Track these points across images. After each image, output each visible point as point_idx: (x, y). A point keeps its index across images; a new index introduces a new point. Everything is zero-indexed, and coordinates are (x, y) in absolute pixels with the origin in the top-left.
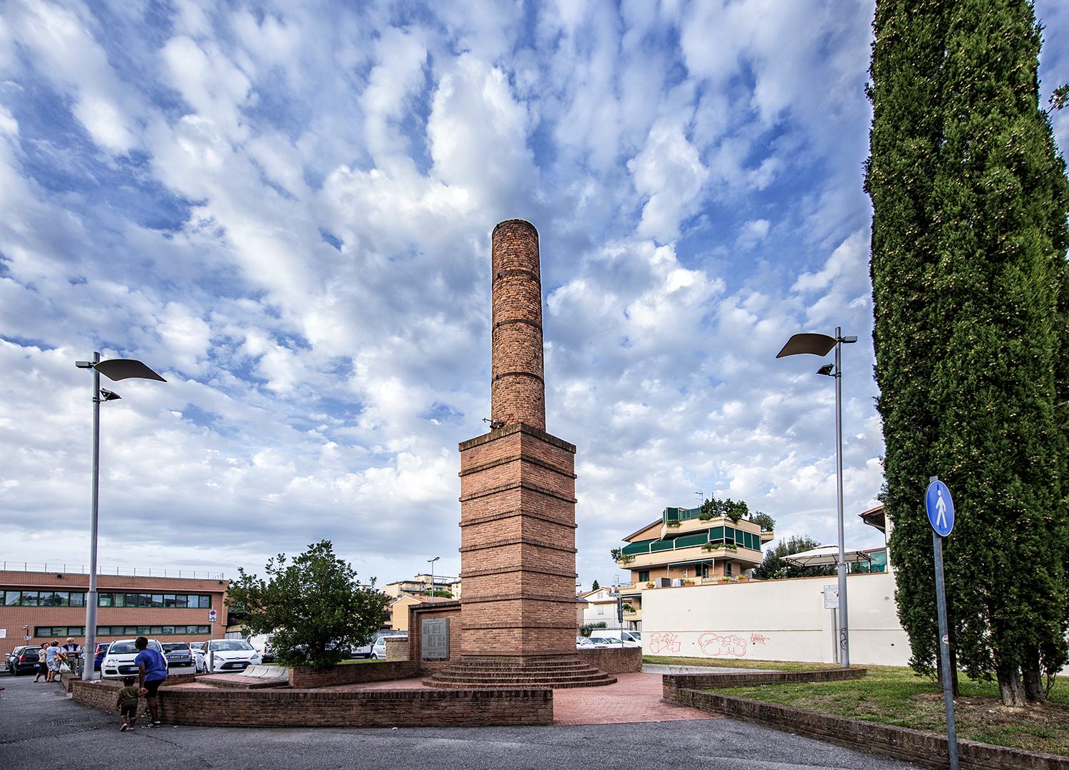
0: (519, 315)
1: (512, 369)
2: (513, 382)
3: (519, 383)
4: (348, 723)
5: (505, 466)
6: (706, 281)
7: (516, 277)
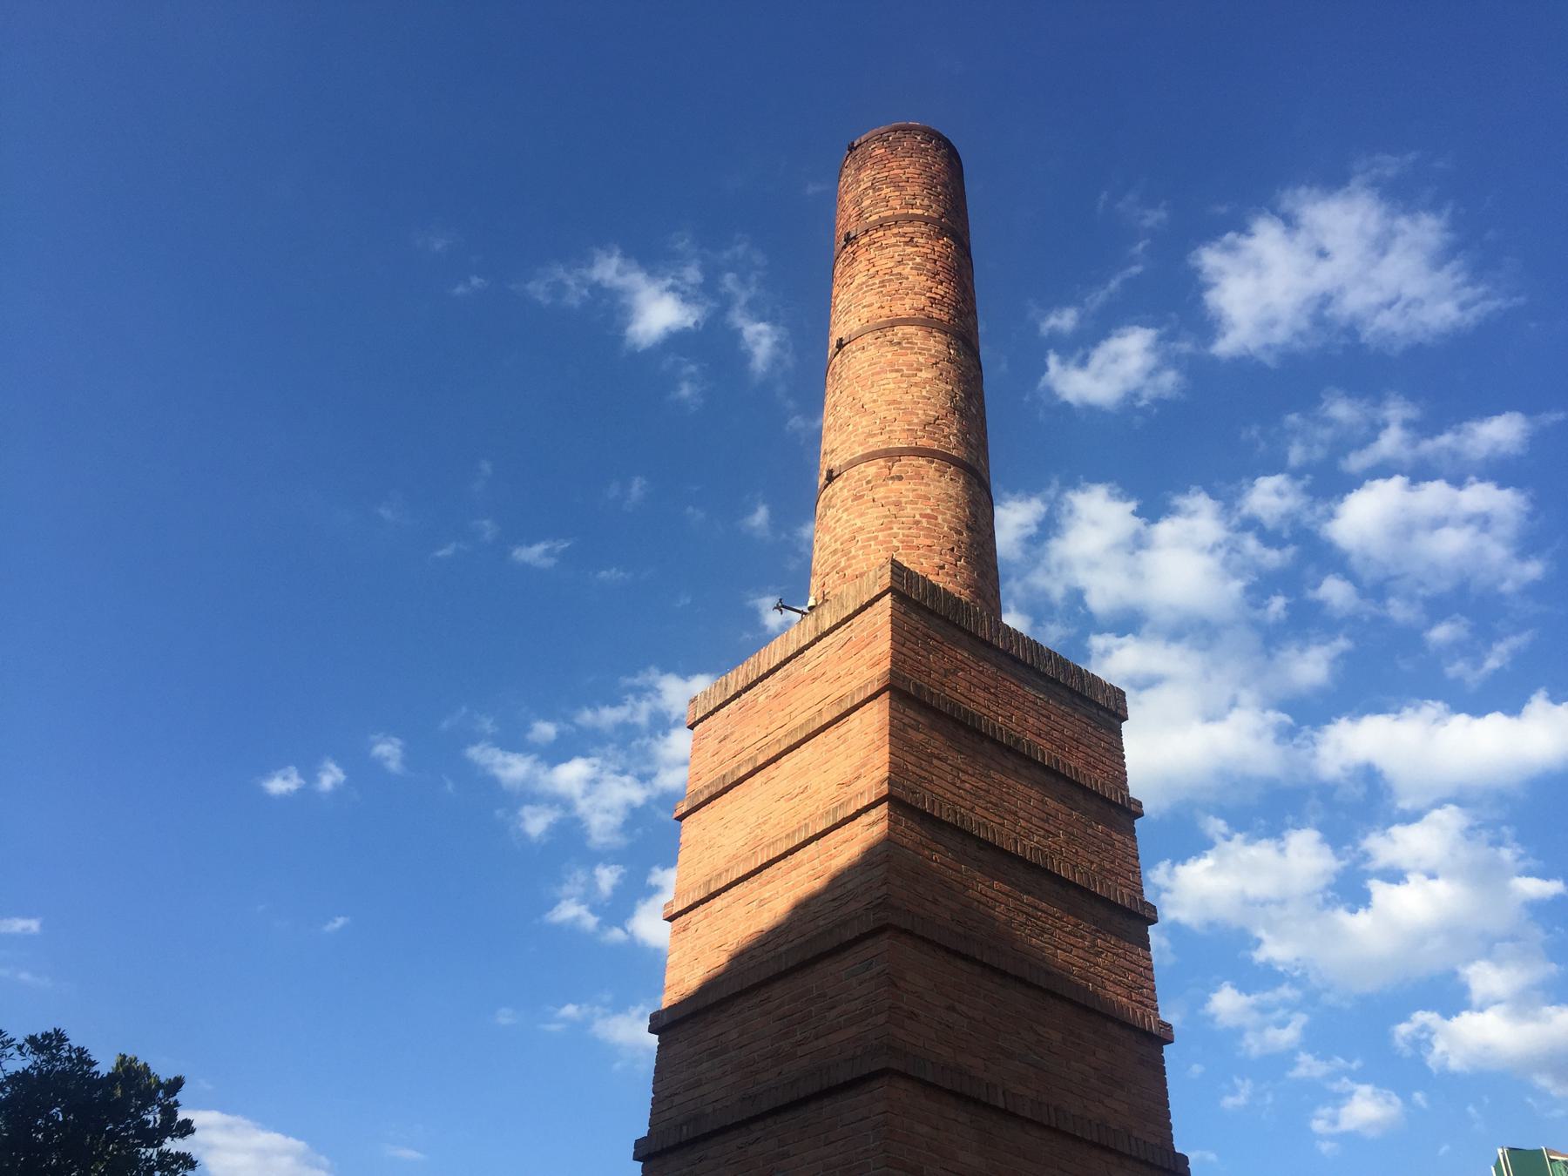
0: (904, 307)
1: (877, 443)
2: (877, 475)
3: (900, 478)
6: (1393, 716)
7: (895, 231)
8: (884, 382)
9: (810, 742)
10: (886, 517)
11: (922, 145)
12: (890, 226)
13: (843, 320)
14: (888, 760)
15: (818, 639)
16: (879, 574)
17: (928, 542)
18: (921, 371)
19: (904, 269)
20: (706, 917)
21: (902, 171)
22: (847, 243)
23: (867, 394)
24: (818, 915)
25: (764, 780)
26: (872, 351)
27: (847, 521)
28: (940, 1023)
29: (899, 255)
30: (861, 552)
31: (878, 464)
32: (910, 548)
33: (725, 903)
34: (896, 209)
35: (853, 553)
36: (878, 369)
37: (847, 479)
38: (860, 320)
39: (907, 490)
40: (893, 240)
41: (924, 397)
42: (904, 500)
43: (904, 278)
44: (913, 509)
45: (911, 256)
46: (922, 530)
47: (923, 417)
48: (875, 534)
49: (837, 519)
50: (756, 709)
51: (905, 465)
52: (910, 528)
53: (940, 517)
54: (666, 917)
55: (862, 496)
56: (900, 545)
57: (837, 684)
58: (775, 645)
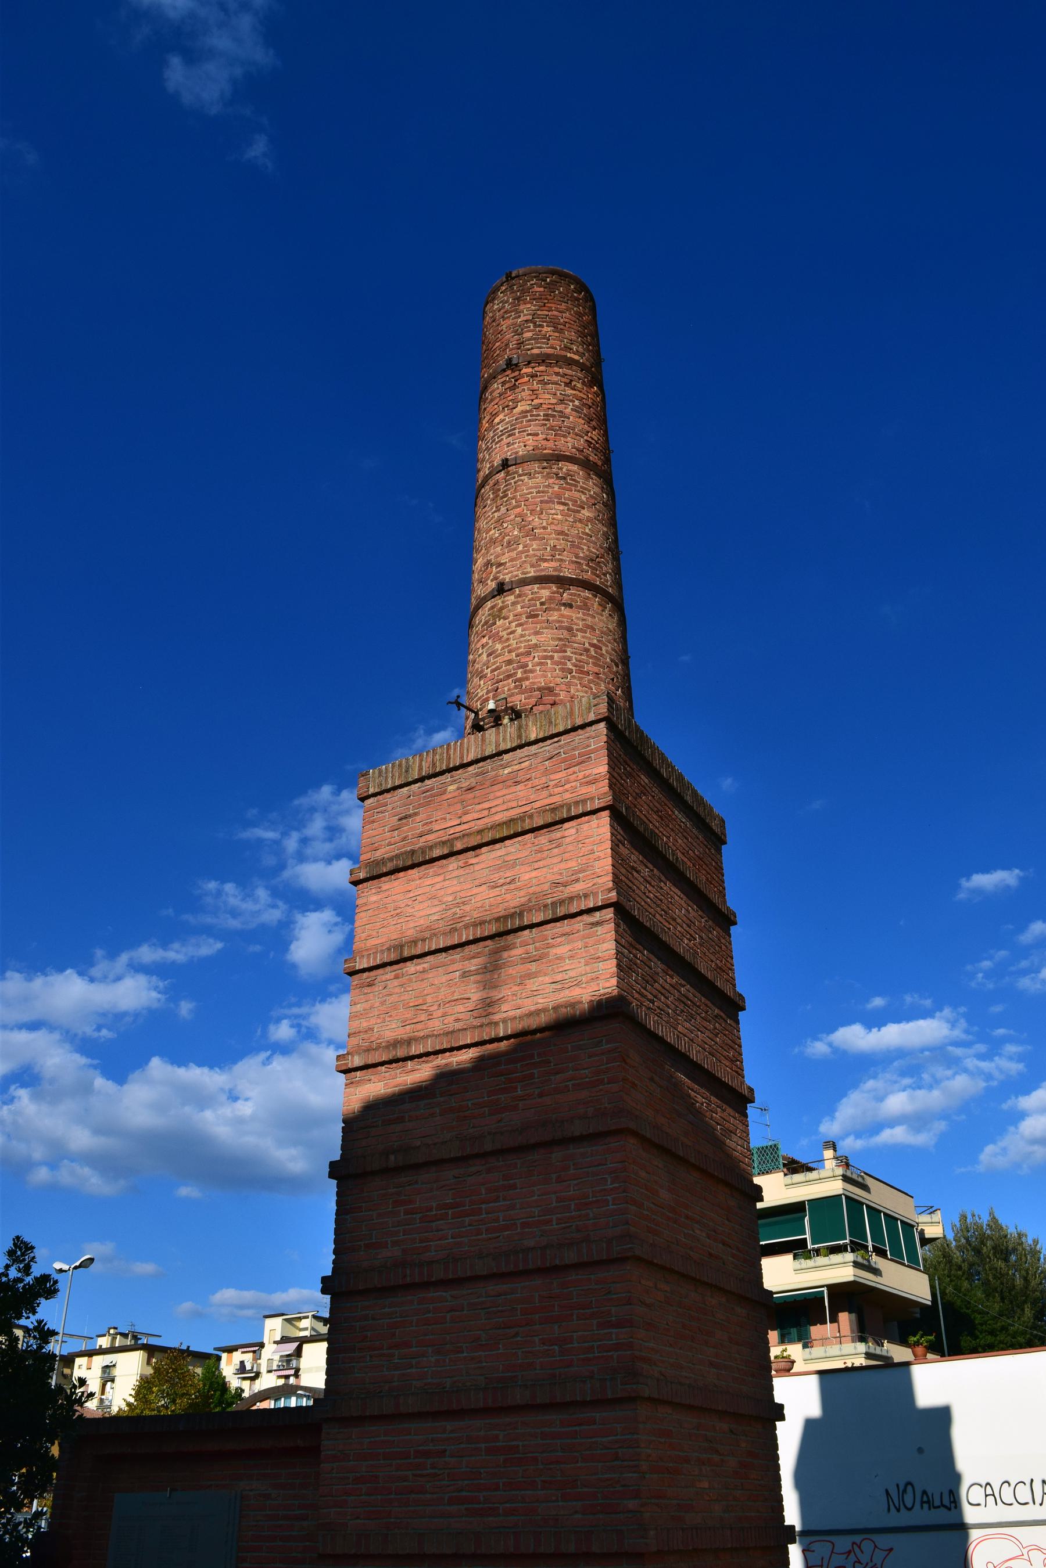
0: (569, 444)
1: (548, 568)
2: (551, 599)
3: (571, 606)
4: (450, 898)
5: (543, 839)
7: (557, 369)
8: (553, 511)
9: (516, 839)
10: (560, 639)
11: (575, 295)
12: (551, 363)
13: (505, 441)
14: (611, 871)
15: (521, 747)
16: (595, 702)
17: (596, 669)
18: (584, 508)
19: (565, 408)
20: (396, 977)
21: (560, 314)
22: (507, 368)
23: (537, 519)
24: (535, 993)
25: (461, 863)
26: (539, 478)
27: (522, 636)
28: (647, 1091)
29: (561, 394)
30: (538, 668)
31: (550, 588)
32: (582, 672)
33: (420, 968)
34: (556, 349)
35: (530, 667)
36: (546, 498)
37: (519, 596)
38: (525, 446)
39: (578, 618)
40: (555, 378)
41: (587, 534)
42: (575, 627)
43: (566, 417)
44: (583, 637)
45: (571, 397)
46: (591, 658)
47: (587, 553)
48: (551, 654)
49: (509, 630)
50: (445, 797)
51: (575, 595)
52: (581, 655)
53: (604, 648)
54: (346, 972)
55: (537, 616)
56: (574, 668)
57: (545, 793)
58: (469, 742)
